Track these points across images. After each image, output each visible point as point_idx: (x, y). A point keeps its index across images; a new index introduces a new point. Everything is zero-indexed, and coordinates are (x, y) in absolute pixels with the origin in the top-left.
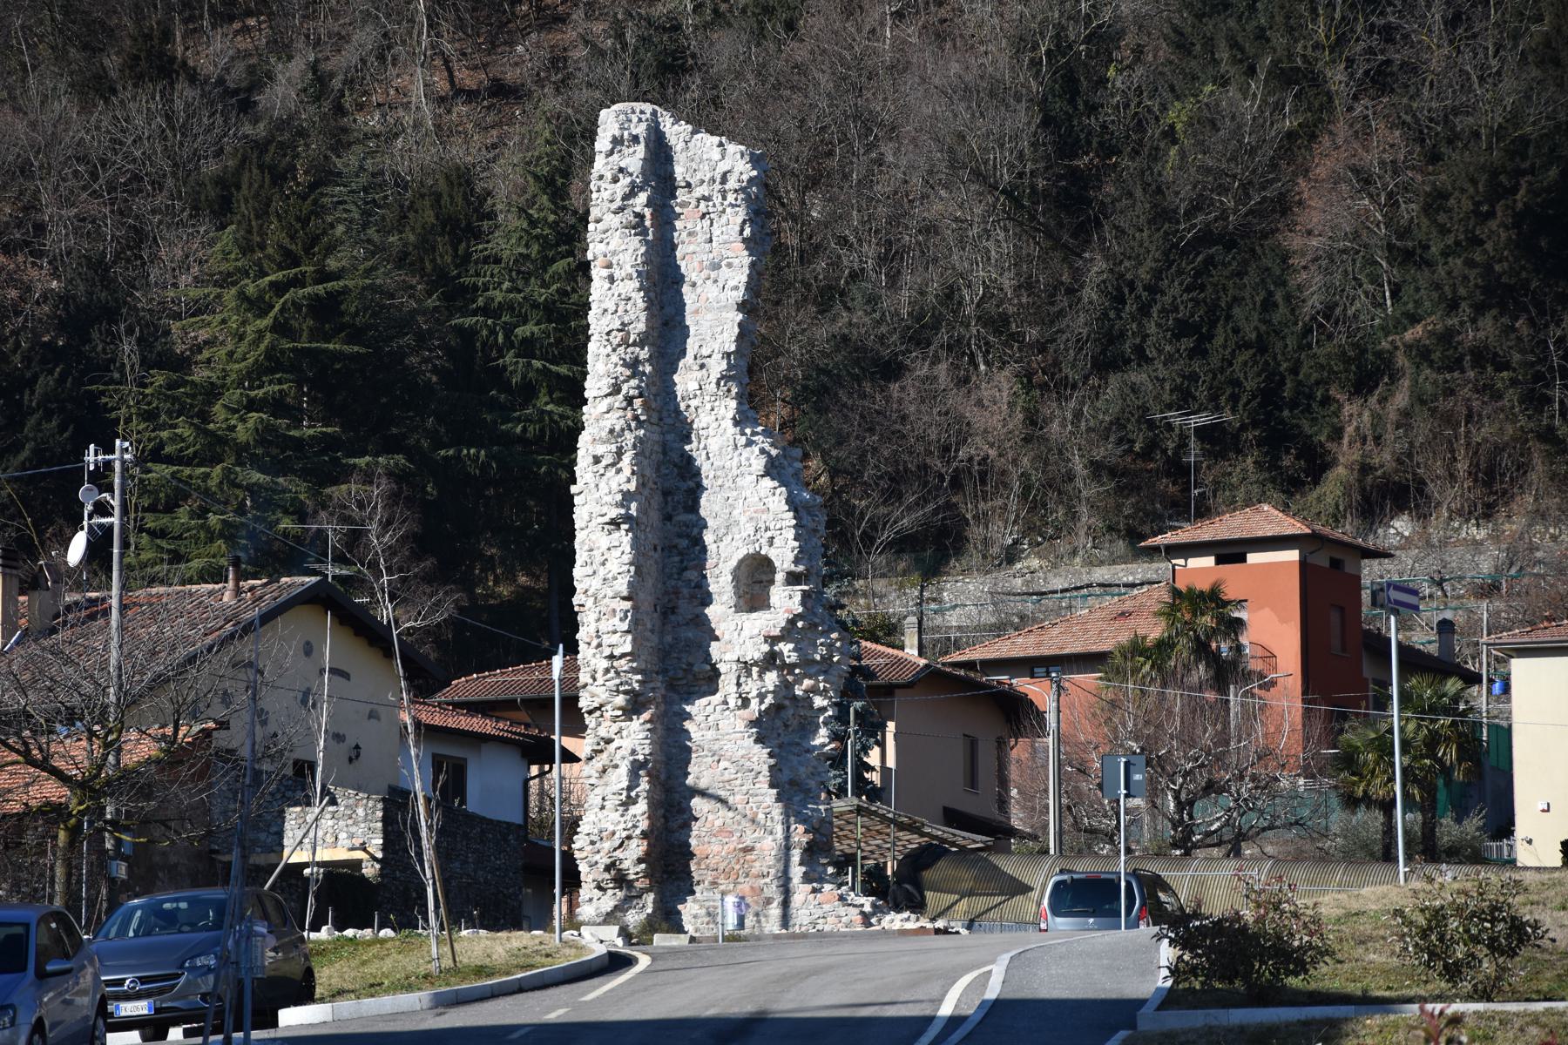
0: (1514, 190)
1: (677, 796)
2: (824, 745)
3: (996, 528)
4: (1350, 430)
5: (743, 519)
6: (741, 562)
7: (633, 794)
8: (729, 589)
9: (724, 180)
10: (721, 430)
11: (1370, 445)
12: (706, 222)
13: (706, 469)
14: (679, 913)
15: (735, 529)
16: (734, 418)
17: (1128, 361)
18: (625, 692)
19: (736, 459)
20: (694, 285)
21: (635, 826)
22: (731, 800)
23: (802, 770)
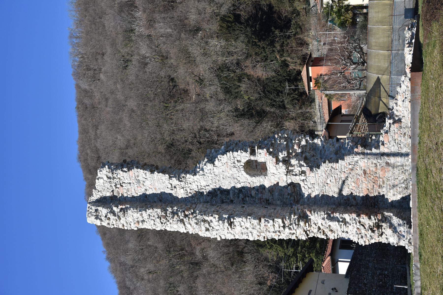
0: (255, 42)
1: (342, 201)
2: (321, 141)
3: (310, 125)
4: (294, 67)
5: (231, 172)
6: (247, 173)
7: (341, 220)
8: (258, 178)
9: (109, 178)
10: (198, 181)
11: (296, 64)
12: (124, 185)
13: (212, 187)
14: (392, 201)
15: (235, 176)
16: (193, 175)
17: (284, 104)
18: (299, 221)
19: (208, 175)
20: (146, 190)
21: (355, 219)
22: (343, 179)
23: (331, 149)
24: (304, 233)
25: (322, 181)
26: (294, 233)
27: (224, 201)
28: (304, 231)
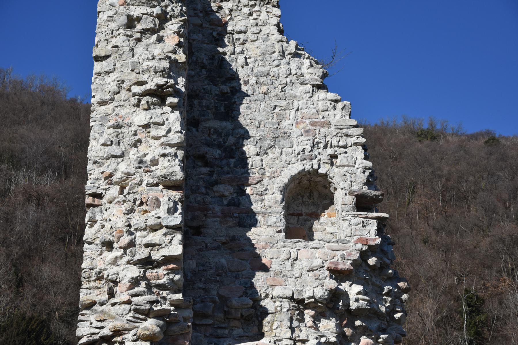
5: (295, 131)
6: (293, 179)
8: (279, 208)
14: (249, 240)
18: (160, 315)
19: (284, 67)
26: (112, 294)
27: (196, 102)
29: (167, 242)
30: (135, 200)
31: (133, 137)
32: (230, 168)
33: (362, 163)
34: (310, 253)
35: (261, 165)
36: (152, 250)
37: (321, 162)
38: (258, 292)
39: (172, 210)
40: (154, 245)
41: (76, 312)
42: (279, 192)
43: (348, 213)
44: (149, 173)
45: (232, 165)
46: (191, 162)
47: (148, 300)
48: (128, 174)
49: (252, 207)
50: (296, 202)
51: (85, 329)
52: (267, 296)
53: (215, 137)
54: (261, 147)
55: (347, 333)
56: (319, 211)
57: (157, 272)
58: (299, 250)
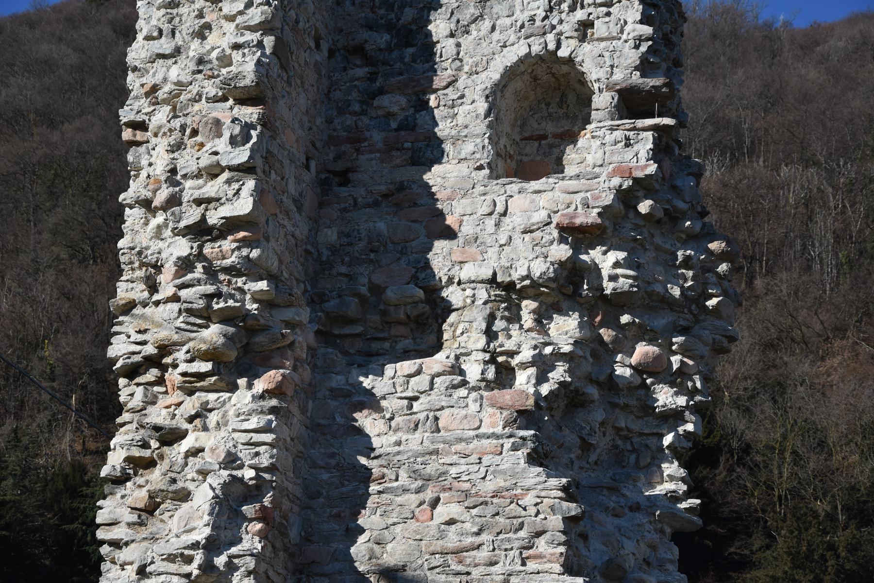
2: (674, 498)
6: (510, 73)
8: (480, 127)
14: (427, 187)
18: (227, 317)
23: (629, 546)
24: (150, 350)
25: (453, 471)
26: (153, 288)
28: (165, 349)
29: (231, 193)
30: (183, 128)
31: (197, 21)
32: (405, 64)
33: (634, 31)
34: (528, 201)
35: (455, 52)
36: (206, 210)
37: (562, 38)
38: (435, 275)
39: (239, 139)
40: (209, 201)
41: (110, 319)
42: (483, 99)
43: (601, 124)
44: (213, 80)
45: (407, 60)
46: (339, 59)
47: (202, 293)
48: (179, 83)
49: (436, 130)
50: (536, 116)
51: (121, 346)
52: (450, 281)
53: (382, 12)
54: (458, 21)
55: (605, 338)
56: (576, 128)
57: (220, 246)
58: (511, 196)
